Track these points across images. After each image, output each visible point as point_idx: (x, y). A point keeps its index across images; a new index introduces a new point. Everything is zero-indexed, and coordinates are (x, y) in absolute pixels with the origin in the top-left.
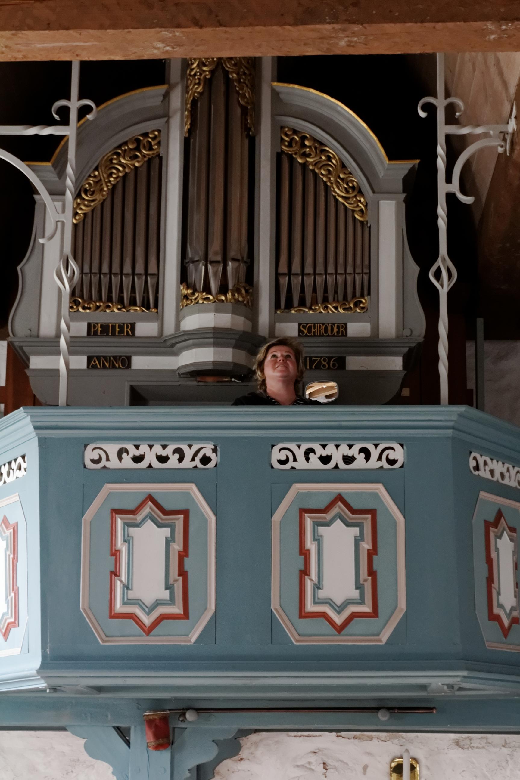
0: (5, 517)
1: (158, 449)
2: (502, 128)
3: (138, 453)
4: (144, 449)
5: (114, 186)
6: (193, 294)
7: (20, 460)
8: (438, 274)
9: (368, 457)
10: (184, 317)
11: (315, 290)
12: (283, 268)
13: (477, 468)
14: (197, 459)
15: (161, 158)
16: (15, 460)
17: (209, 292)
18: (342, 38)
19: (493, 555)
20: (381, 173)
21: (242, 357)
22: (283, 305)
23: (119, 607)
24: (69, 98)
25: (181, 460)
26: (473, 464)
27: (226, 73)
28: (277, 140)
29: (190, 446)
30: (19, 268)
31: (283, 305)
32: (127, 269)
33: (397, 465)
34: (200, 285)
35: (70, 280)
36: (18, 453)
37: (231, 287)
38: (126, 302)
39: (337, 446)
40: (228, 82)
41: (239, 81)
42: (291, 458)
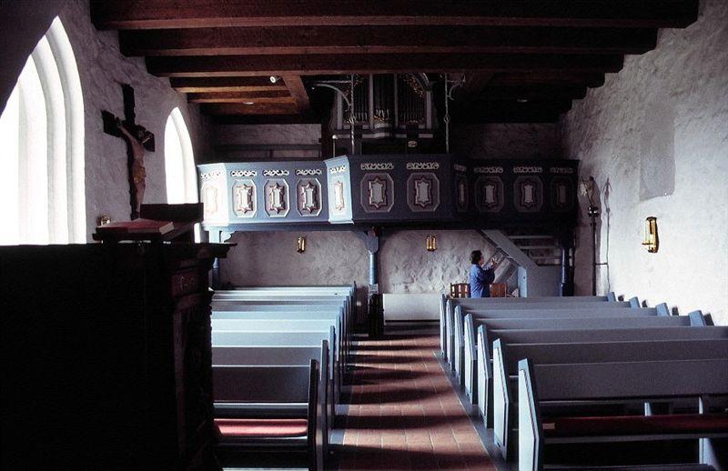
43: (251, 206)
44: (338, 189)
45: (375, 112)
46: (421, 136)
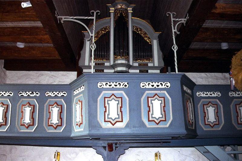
1: (115, 83)
3: (110, 84)
4: (111, 83)
7: (83, 86)
8: (173, 48)
9: (162, 85)
19: (81, 117)
25: (120, 86)
33: (169, 87)
39: (155, 83)
42: (145, 85)
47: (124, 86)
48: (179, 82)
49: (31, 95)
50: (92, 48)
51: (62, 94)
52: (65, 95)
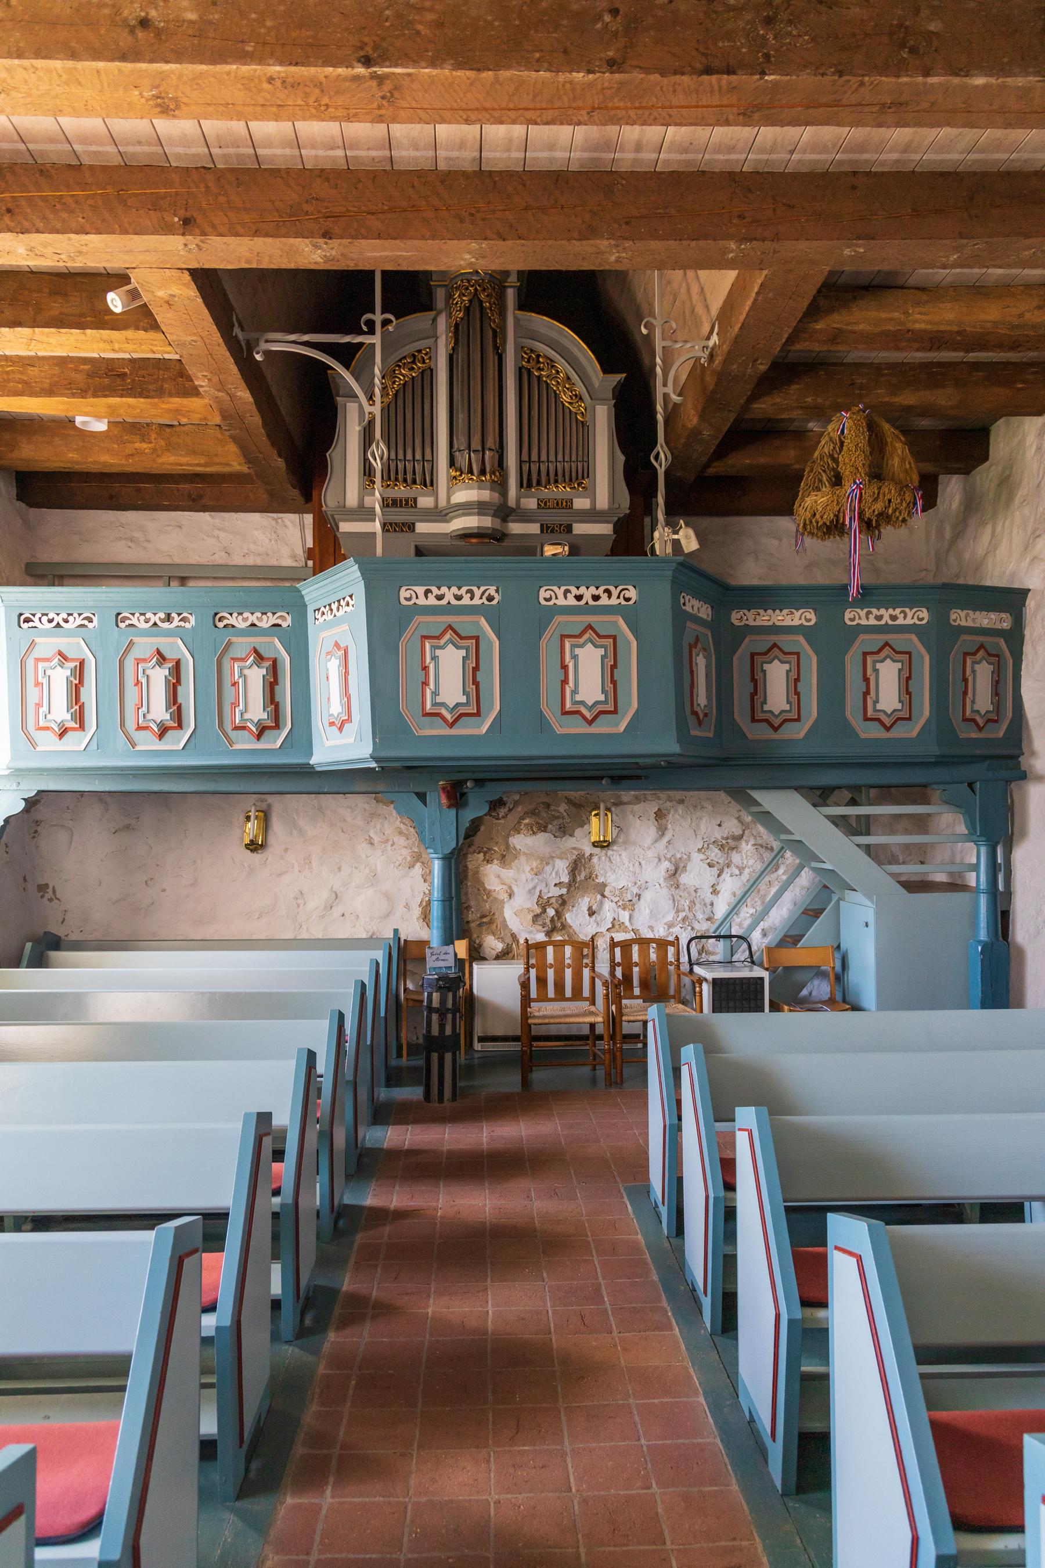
0: (336, 642)
1: (454, 589)
2: (705, 343)
4: (444, 589)
5: (397, 391)
6: (461, 475)
7: (348, 598)
8: (657, 458)
9: (610, 597)
10: (454, 493)
11: (548, 474)
12: (525, 458)
13: (684, 604)
14: (484, 597)
15: (432, 370)
16: (344, 599)
17: (472, 474)
18: (614, 253)
19: (695, 669)
20: (597, 385)
21: (498, 524)
22: (525, 485)
23: (568, 705)
24: (373, 312)
25: (472, 599)
26: (682, 601)
27: (481, 302)
28: (519, 357)
29: (479, 588)
30: (327, 454)
31: (525, 485)
32: (409, 456)
33: (631, 602)
34: (466, 469)
35: (381, 459)
36: (346, 593)
37: (488, 470)
38: (409, 481)
39: (588, 588)
40: (481, 308)
41: (491, 310)
43: (80, 718)
44: (334, 666)
45: (452, 463)
46: (580, 529)
47: (484, 600)
48: (668, 586)
49: (166, 625)
50: (375, 459)
51: (273, 620)
52: (284, 625)
